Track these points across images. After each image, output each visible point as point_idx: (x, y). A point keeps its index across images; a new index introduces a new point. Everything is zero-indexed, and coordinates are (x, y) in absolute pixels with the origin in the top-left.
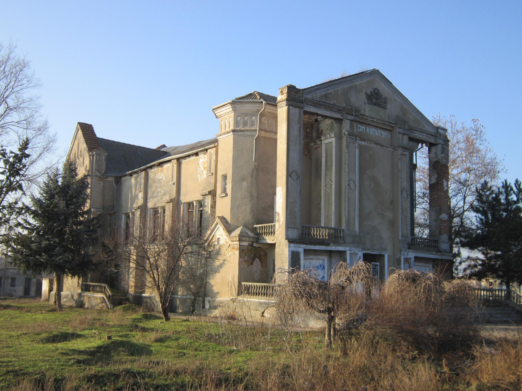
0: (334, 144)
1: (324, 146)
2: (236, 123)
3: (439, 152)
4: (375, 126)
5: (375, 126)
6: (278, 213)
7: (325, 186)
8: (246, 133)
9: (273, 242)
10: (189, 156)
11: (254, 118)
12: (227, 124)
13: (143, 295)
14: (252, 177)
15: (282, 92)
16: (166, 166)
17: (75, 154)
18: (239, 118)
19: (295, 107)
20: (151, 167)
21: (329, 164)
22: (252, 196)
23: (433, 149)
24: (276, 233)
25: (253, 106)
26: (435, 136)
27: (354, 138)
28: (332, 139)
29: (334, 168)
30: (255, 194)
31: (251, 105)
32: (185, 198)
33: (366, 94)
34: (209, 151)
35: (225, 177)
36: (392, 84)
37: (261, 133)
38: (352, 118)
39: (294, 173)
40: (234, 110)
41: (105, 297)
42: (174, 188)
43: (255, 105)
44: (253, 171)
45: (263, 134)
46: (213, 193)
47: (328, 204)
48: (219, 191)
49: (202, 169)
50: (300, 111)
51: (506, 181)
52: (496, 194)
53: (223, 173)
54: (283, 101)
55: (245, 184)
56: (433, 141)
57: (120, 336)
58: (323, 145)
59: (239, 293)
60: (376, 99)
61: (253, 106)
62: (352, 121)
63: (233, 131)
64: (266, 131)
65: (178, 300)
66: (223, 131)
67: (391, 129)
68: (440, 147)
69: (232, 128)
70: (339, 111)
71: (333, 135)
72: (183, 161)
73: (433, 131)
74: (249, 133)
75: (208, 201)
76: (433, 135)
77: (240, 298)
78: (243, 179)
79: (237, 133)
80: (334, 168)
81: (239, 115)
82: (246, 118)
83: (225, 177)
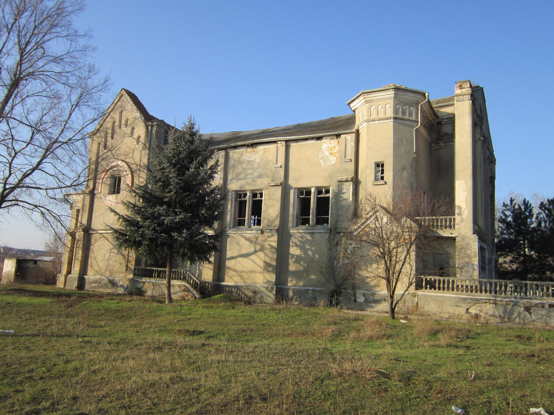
2: (396, 111)
6: (460, 208)
8: (406, 122)
10: (306, 139)
13: (223, 283)
14: (412, 168)
16: (261, 148)
18: (398, 106)
20: (236, 147)
22: (412, 187)
24: (456, 226)
30: (415, 186)
31: (413, 95)
32: (295, 182)
34: (342, 136)
35: (380, 166)
36: (485, 102)
41: (188, 286)
42: (282, 172)
43: (416, 96)
44: (412, 162)
51: (512, 201)
52: (119, 235)
53: (378, 160)
54: (465, 95)
55: (405, 174)
59: (419, 286)
72: (293, 145)
74: (409, 123)
77: (420, 292)
78: (404, 169)
79: (397, 121)
81: (398, 102)
82: (405, 107)
83: (380, 166)
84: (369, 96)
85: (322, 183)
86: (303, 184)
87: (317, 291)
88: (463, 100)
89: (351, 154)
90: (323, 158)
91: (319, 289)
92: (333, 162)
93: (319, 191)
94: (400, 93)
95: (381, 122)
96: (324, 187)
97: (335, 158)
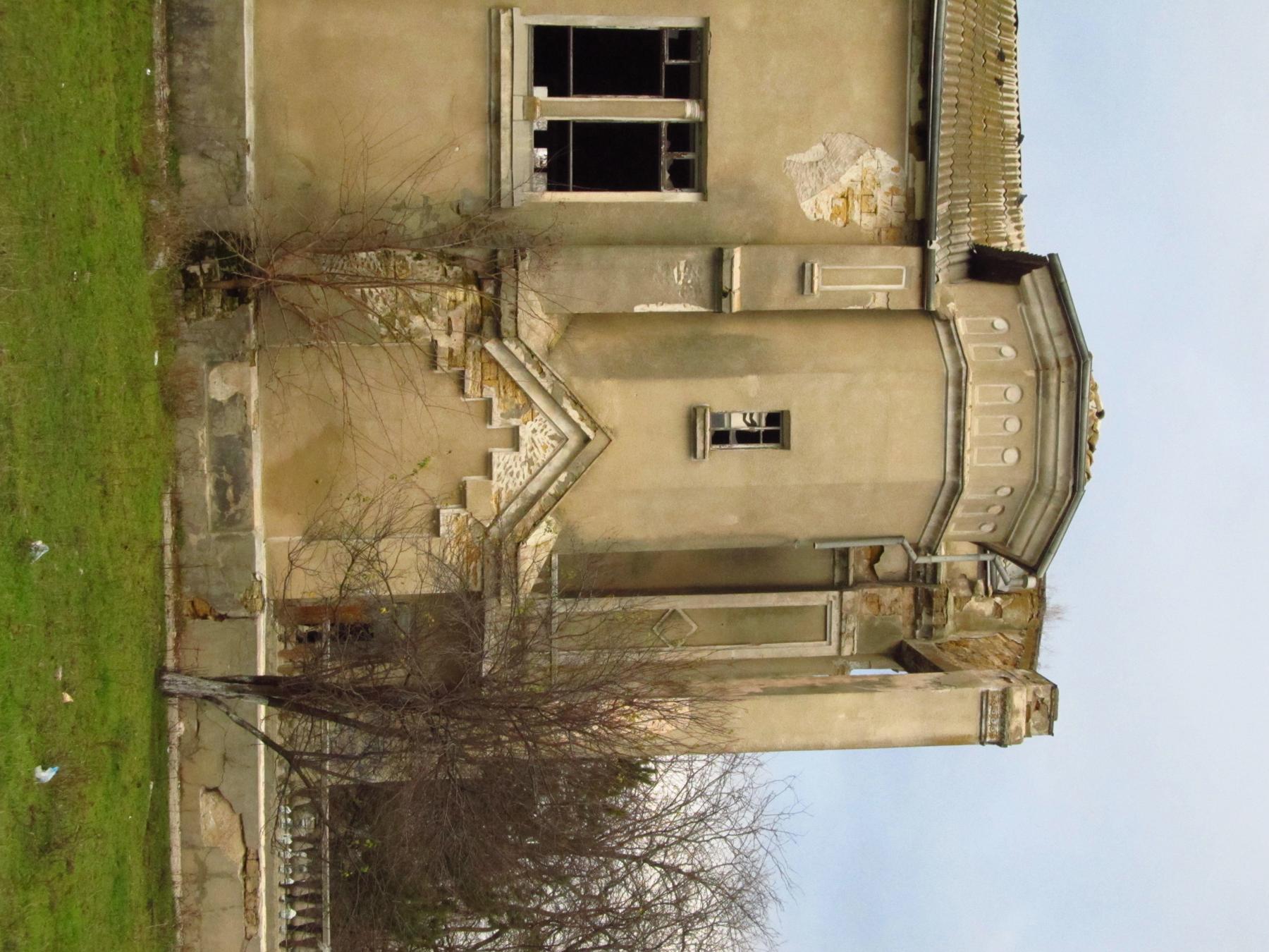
8: (934, 517)
49: (850, 175)
53: (795, 425)
54: (1003, 724)
85: (723, 152)
86: (722, 65)
87: (240, 162)
88: (983, 716)
89: (827, 286)
90: (831, 155)
91: (250, 165)
92: (807, 206)
93: (687, 136)
95: (950, 431)
96: (703, 158)
97: (826, 214)
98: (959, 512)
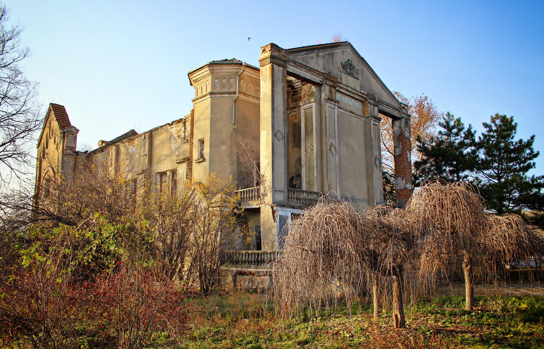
0: (314, 110)
1: (302, 111)
2: (213, 86)
3: (403, 125)
4: (349, 96)
5: (349, 96)
7: (306, 151)
8: (224, 95)
9: (257, 207)
11: (232, 80)
12: (204, 88)
15: (264, 51)
17: (47, 134)
19: (279, 65)
21: (308, 129)
23: (397, 123)
25: (227, 75)
26: (399, 111)
27: (333, 103)
28: (312, 104)
29: (314, 132)
33: (342, 64)
37: (240, 96)
38: (331, 84)
39: (279, 132)
40: (212, 72)
45: (242, 96)
46: (188, 160)
47: (310, 170)
48: (196, 156)
50: (283, 70)
56: (398, 116)
57: (361, 93)
58: (302, 111)
60: (350, 69)
61: (227, 75)
62: (331, 86)
63: (211, 93)
64: (245, 94)
65: (526, 193)
66: (200, 95)
67: (363, 100)
68: (403, 120)
69: (209, 90)
70: (319, 74)
71: (313, 100)
73: (397, 106)
75: (182, 170)
76: (397, 110)
78: (222, 143)
80: (314, 132)
83: (202, 142)
84: (194, 75)
94: (216, 68)
98: (225, 90)
